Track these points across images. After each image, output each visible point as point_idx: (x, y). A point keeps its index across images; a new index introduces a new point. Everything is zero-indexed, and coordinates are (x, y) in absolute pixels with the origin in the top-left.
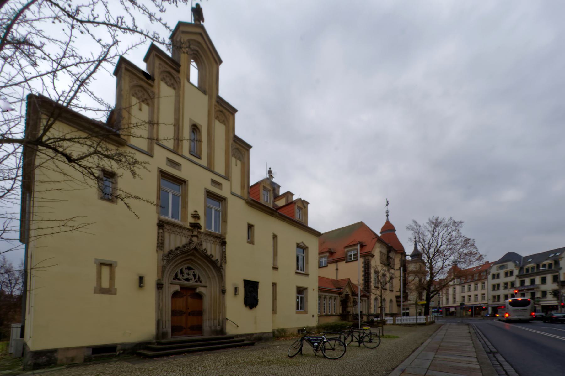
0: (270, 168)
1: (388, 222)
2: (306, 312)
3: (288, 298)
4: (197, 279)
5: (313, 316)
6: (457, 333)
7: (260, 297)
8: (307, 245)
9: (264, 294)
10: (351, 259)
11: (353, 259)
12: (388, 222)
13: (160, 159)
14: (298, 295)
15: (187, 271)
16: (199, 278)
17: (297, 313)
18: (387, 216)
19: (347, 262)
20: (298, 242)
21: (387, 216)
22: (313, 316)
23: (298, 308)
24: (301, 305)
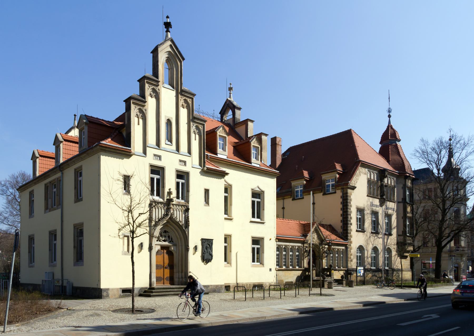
0: (170, 189)
1: (389, 126)
2: (262, 263)
3: (242, 248)
4: (170, 240)
5: (270, 270)
6: (355, 267)
7: (214, 253)
8: (263, 189)
9: (218, 250)
10: (297, 196)
11: (299, 197)
12: (389, 126)
13: (150, 160)
14: (254, 246)
15: (165, 234)
16: (172, 239)
17: (253, 266)
18: (389, 116)
19: (294, 199)
20: (253, 187)
21: (389, 116)
22: (270, 270)
23: (253, 261)
24: (257, 255)
